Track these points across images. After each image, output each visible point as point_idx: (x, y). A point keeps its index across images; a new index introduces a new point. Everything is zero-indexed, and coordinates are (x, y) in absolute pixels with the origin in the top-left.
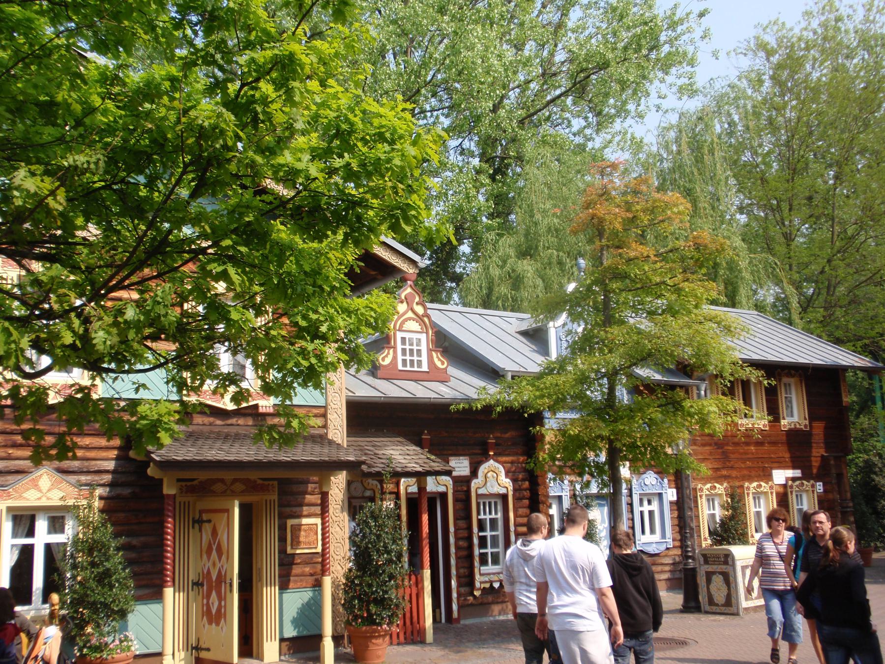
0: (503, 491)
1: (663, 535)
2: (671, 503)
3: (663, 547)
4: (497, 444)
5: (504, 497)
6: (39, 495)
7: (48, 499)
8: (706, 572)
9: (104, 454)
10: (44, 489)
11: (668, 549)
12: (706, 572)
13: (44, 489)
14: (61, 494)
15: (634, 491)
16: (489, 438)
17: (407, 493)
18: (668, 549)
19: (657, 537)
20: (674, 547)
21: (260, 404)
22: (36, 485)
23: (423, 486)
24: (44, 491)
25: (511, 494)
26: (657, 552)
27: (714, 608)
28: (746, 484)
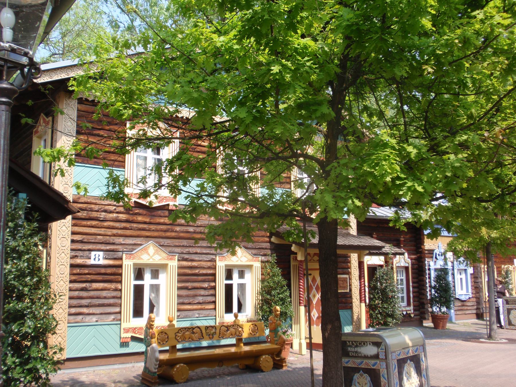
0: (407, 265)
1: (467, 291)
2: (471, 274)
3: (467, 297)
4: (404, 241)
5: (407, 268)
6: (237, 259)
7: (241, 261)
8: (508, 309)
9: (262, 239)
10: (151, 254)
11: (469, 298)
12: (508, 309)
13: (151, 254)
14: (160, 258)
15: (455, 268)
16: (401, 238)
17: (368, 265)
18: (469, 298)
19: (464, 292)
20: (472, 297)
21: (170, 204)
22: (147, 252)
23: (362, 260)
24: (151, 255)
25: (410, 266)
26: (465, 299)
27: (512, 327)
28: (503, 266)
